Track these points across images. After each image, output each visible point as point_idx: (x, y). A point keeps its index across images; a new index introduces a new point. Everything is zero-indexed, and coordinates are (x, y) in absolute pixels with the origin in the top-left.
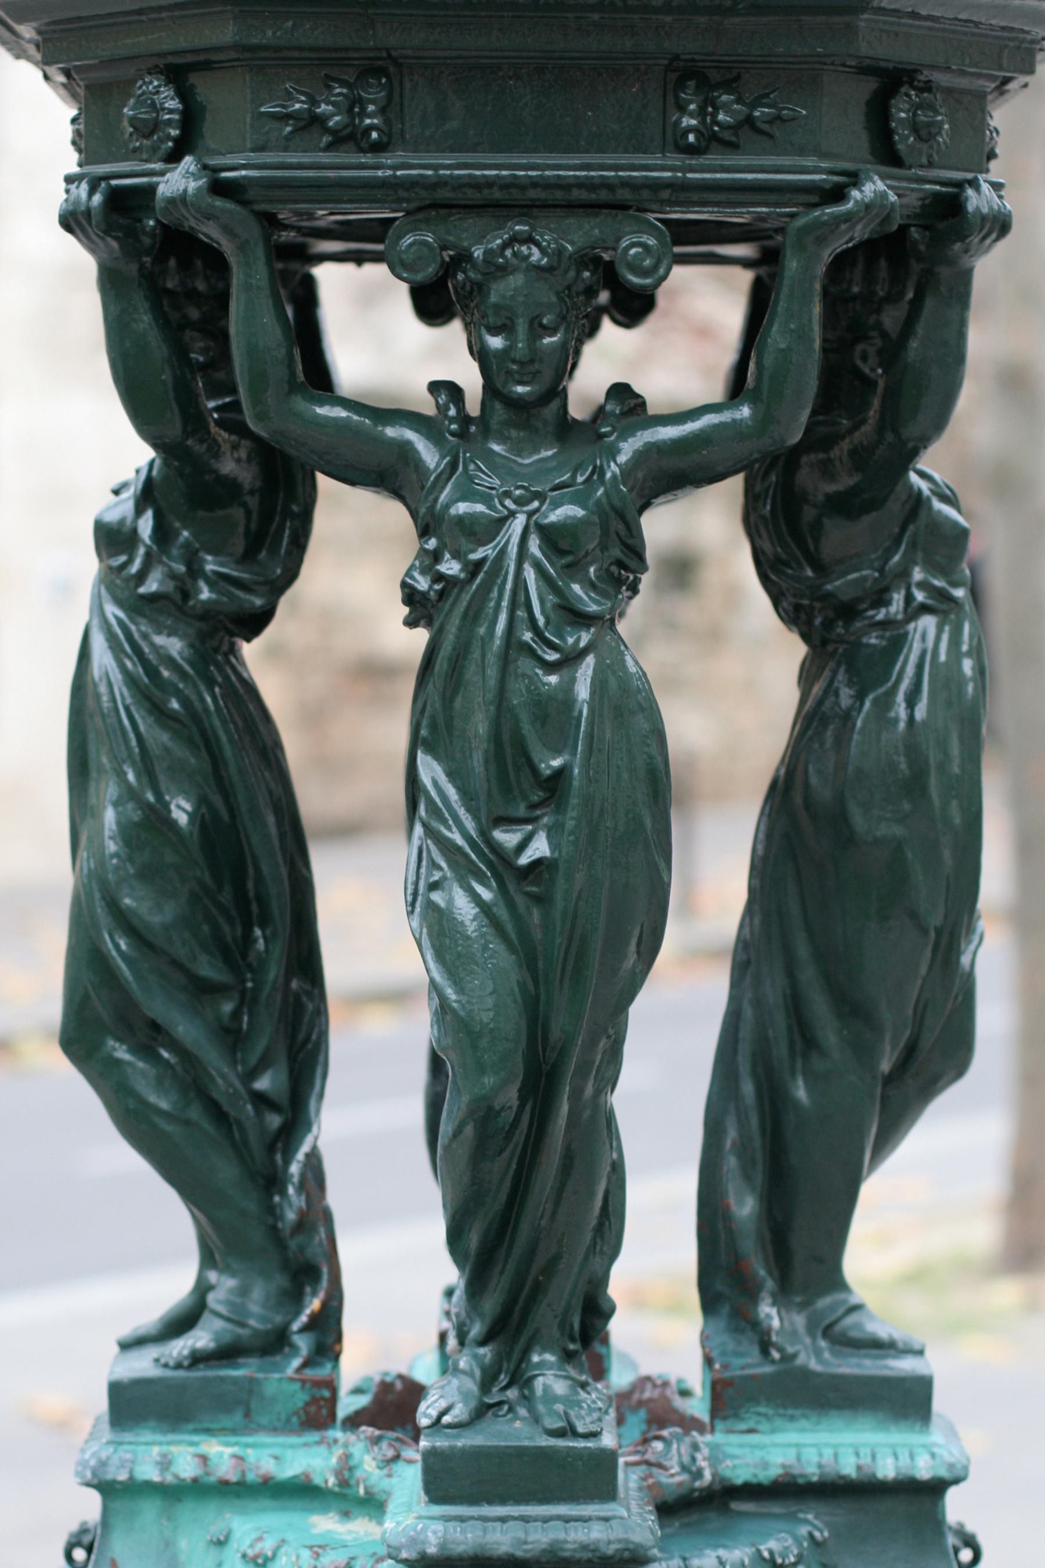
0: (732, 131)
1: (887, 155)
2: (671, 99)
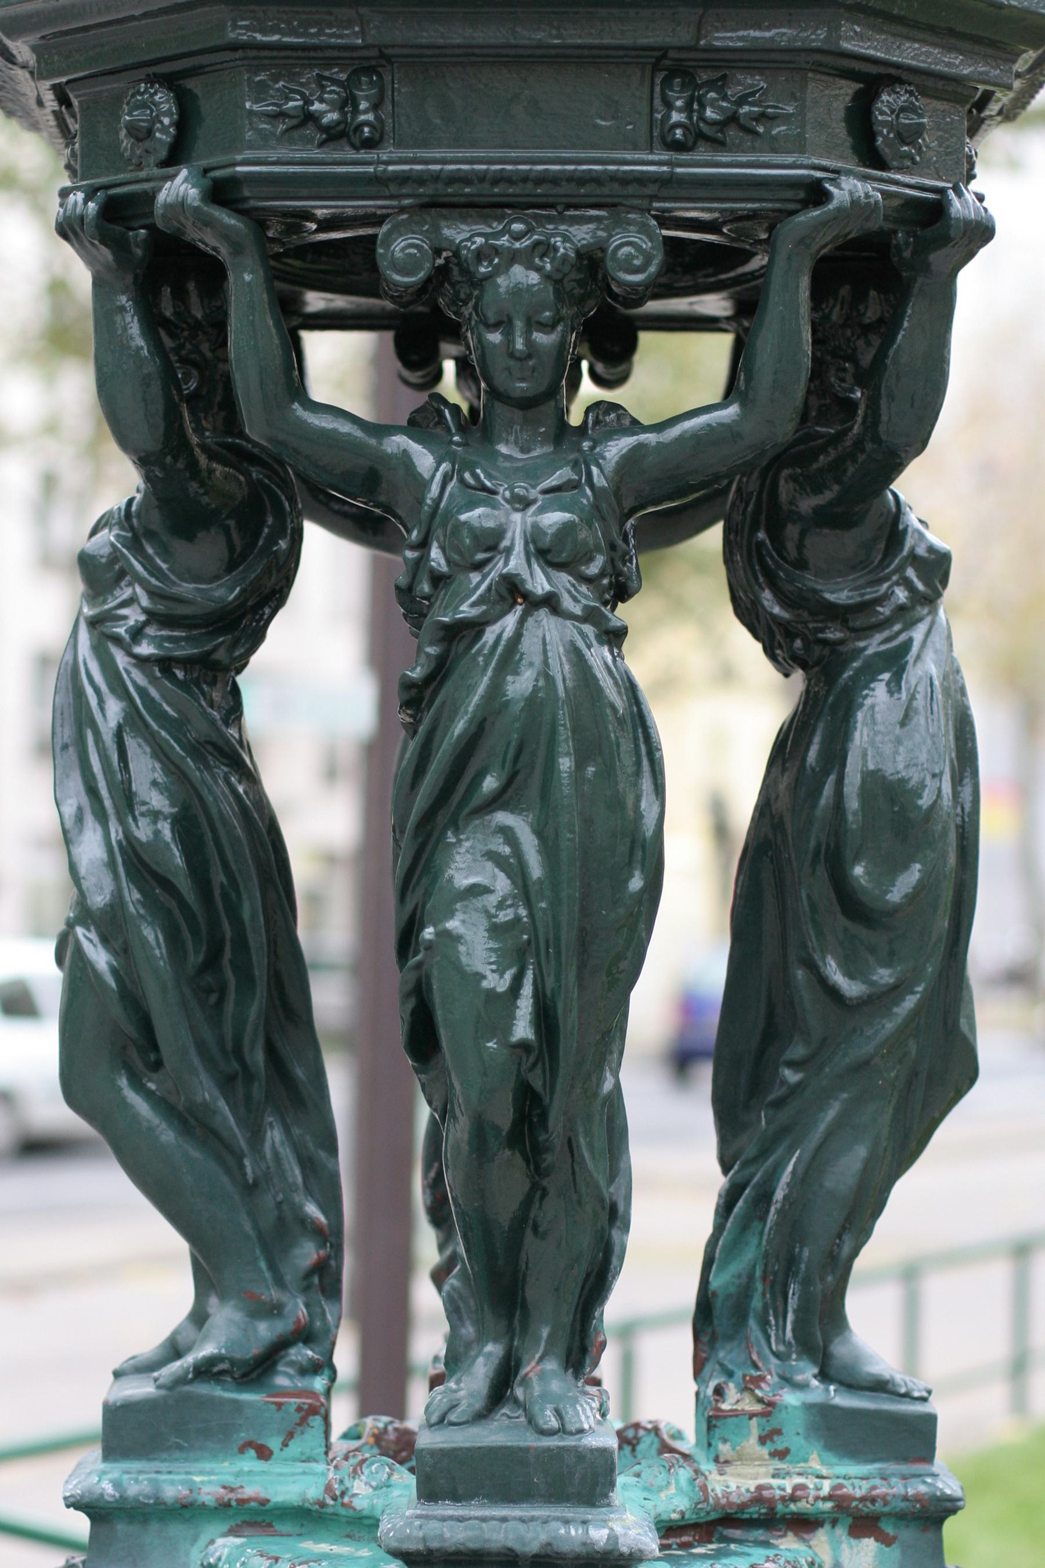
0: (719, 127)
1: (870, 156)
2: (657, 102)
